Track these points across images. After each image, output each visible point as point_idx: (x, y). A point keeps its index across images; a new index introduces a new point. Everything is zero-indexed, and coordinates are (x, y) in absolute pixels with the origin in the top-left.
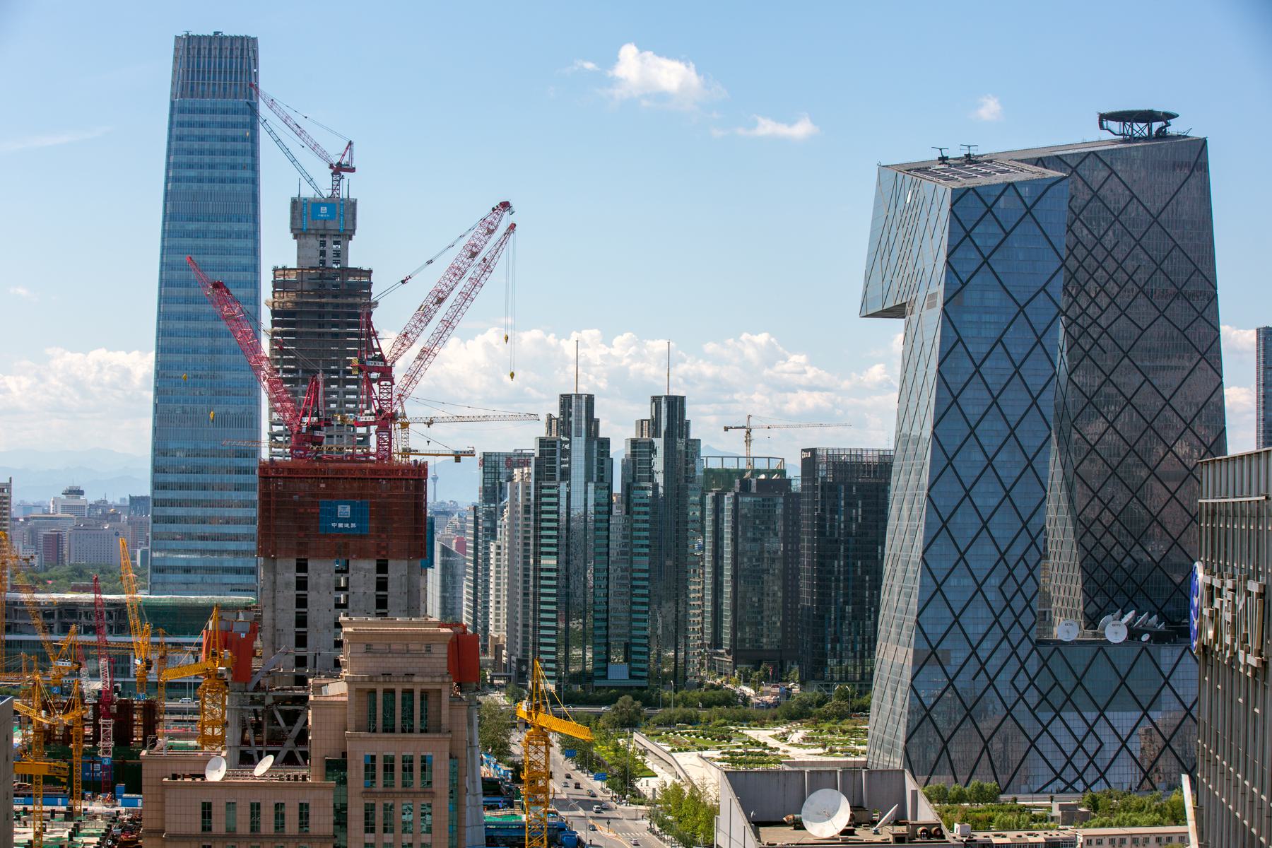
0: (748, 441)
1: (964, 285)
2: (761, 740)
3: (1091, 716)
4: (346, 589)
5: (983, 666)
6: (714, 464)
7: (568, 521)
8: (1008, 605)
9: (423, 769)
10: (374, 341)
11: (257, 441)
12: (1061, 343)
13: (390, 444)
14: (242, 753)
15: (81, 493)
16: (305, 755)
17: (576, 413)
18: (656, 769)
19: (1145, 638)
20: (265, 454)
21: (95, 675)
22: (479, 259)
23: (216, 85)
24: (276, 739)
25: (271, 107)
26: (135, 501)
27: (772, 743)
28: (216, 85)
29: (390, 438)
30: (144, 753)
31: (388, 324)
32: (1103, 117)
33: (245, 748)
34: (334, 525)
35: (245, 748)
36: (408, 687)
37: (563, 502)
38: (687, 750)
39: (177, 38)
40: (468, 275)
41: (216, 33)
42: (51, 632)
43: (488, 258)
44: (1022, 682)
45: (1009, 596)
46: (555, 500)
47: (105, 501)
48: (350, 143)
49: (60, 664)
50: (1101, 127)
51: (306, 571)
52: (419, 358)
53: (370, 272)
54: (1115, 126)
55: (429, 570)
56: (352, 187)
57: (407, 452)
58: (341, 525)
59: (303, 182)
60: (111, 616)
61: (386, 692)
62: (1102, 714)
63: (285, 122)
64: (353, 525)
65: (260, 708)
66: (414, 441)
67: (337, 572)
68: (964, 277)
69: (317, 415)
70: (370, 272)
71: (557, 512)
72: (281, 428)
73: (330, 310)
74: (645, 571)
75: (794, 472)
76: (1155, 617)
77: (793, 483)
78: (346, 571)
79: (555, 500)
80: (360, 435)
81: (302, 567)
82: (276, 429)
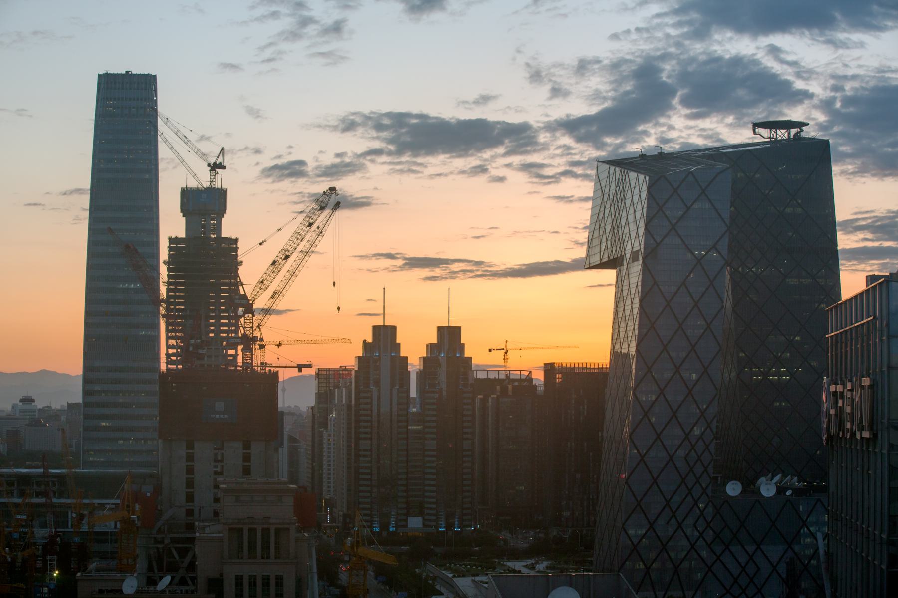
0: (506, 359)
1: (658, 244)
2: (517, 568)
3: (751, 549)
4: (221, 461)
5: (674, 515)
6: (481, 375)
7: (379, 415)
8: (691, 470)
9: (277, 584)
10: (241, 288)
11: (158, 359)
12: (727, 285)
13: (252, 359)
14: (149, 578)
15: (33, 401)
16: (193, 579)
17: (384, 337)
18: (443, 590)
19: (789, 493)
20: (163, 367)
21: (44, 525)
22: (314, 227)
23: (126, 110)
24: (172, 568)
25: (166, 124)
26: (71, 406)
27: (525, 571)
28: (126, 110)
29: (252, 355)
30: (79, 574)
31: (250, 272)
32: (756, 125)
33: (150, 574)
34: (213, 416)
35: (150, 574)
36: (266, 526)
37: (375, 402)
38: (464, 576)
39: (100, 76)
40: (306, 239)
41: (127, 72)
42: (13, 496)
43: (321, 226)
44: (701, 526)
45: (692, 464)
46: (369, 400)
47: (50, 407)
48: (223, 149)
49: (19, 517)
50: (755, 132)
51: (192, 448)
52: (272, 297)
53: (237, 239)
54: (765, 132)
55: (280, 449)
56: (223, 180)
57: (264, 365)
58: (217, 416)
59: (189, 176)
60: (55, 485)
61: (250, 530)
62: (759, 547)
63: (176, 134)
64: (226, 416)
65: (160, 546)
66: (266, 357)
67: (215, 449)
68: (658, 239)
69: (200, 338)
70: (237, 239)
71: (371, 416)
72: (175, 351)
73: (209, 258)
74: (433, 450)
75: (539, 377)
76: (796, 479)
77: (538, 389)
78: (221, 449)
79: (369, 400)
80: (231, 356)
81: (190, 446)
82: (171, 351)
